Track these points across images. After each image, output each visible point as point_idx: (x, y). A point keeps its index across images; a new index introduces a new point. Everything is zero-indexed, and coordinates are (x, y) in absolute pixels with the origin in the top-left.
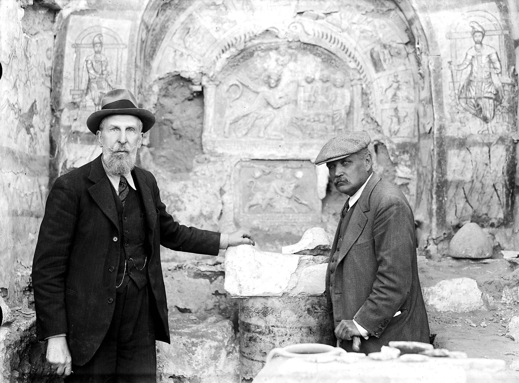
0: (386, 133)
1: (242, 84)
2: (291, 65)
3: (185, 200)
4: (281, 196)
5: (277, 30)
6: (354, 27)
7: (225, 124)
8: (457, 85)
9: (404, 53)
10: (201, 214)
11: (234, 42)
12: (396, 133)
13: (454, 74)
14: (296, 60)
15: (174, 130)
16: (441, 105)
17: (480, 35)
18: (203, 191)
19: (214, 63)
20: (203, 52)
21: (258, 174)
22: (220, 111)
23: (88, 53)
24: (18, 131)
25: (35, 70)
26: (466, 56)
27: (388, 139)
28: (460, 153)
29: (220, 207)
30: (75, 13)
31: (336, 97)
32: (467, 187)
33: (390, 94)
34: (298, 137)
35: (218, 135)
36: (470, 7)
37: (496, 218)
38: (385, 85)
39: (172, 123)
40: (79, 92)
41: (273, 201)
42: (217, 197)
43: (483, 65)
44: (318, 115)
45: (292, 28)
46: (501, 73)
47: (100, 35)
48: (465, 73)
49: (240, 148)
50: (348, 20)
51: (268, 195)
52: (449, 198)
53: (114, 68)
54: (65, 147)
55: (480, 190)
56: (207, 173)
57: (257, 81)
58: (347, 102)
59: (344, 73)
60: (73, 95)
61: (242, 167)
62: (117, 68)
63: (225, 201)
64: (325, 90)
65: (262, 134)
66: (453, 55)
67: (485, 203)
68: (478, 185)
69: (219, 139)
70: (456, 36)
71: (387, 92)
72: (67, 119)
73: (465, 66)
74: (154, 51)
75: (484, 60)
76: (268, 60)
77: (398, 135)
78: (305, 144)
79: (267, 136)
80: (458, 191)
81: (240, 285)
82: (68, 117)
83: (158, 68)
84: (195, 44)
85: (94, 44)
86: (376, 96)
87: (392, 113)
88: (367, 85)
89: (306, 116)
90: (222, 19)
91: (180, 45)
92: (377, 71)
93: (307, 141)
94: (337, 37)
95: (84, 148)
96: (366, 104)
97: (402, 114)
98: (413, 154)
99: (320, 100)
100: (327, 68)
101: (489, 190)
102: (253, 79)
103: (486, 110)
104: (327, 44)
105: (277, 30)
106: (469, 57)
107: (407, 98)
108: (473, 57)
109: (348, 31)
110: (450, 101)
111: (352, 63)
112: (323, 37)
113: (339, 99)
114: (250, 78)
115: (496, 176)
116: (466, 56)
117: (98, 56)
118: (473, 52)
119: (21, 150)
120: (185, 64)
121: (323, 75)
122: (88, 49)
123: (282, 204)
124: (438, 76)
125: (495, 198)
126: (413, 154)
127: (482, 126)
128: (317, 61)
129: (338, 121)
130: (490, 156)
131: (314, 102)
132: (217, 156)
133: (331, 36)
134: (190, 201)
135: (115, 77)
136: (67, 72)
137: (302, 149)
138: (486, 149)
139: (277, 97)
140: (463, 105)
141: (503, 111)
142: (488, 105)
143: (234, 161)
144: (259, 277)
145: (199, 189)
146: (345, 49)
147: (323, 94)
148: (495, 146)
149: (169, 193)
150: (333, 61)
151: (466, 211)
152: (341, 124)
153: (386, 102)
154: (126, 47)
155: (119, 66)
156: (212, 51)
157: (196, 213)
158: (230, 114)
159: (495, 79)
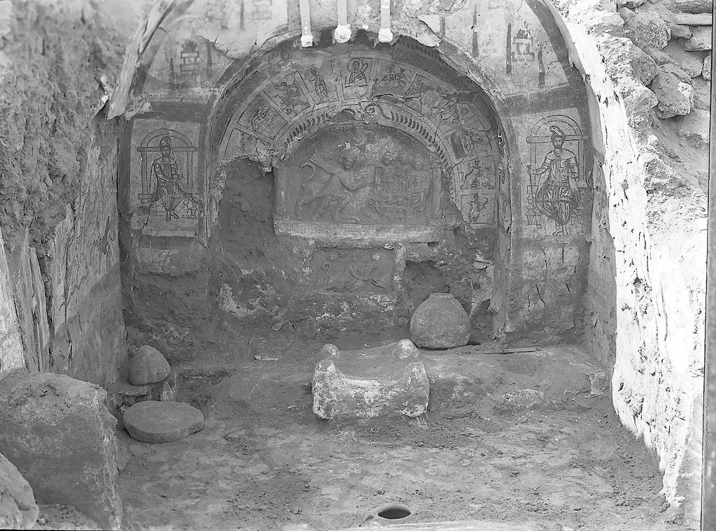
0: (466, 218)
5: (354, 112)
8: (535, 189)
11: (307, 124)
12: (475, 219)
13: (533, 178)
14: (372, 142)
16: (519, 207)
17: (558, 139)
20: (273, 135)
23: (153, 156)
30: (138, 116)
33: (470, 180)
46: (578, 177)
47: (167, 138)
60: (142, 199)
70: (536, 140)
73: (544, 170)
74: (220, 135)
77: (478, 221)
85: (161, 147)
90: (293, 100)
92: (458, 157)
96: (446, 183)
97: (482, 200)
107: (488, 184)
109: (430, 116)
117: (167, 159)
118: (552, 156)
124: (518, 179)
135: (186, 181)
138: (560, 250)
140: (540, 208)
146: (424, 133)
154: (196, 150)
159: (573, 184)
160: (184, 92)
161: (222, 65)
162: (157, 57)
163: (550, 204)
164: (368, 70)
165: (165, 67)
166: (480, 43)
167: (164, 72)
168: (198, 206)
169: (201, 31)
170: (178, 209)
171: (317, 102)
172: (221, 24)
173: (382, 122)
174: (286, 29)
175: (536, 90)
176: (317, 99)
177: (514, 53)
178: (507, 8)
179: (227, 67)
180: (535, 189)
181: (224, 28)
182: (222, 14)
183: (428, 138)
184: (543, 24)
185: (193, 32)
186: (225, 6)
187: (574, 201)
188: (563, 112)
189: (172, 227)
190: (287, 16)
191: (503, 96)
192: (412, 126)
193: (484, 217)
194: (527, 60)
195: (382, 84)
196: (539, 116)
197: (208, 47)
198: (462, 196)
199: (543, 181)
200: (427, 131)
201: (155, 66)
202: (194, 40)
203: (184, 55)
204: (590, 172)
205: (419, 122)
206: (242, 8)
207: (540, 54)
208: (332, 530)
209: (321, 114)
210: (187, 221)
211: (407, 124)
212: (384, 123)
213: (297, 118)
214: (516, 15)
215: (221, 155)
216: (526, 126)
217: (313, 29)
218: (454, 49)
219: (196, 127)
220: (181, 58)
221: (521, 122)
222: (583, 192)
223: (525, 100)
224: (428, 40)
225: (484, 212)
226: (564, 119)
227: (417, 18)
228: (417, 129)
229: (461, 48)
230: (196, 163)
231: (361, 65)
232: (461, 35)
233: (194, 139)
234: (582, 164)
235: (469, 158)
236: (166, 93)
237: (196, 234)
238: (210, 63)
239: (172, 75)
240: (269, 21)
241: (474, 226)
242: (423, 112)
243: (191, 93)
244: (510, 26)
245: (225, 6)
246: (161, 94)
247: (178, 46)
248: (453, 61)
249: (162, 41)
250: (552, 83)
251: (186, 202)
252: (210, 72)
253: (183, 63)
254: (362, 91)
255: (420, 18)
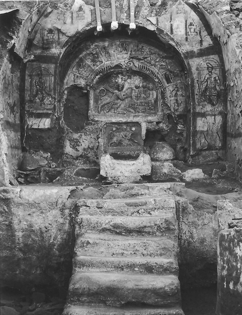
0: (172, 110)
1: (106, 90)
2: (129, 81)
3: (81, 141)
4: (125, 139)
5: (122, 65)
6: (157, 63)
7: (99, 107)
8: (201, 90)
9: (180, 75)
10: (89, 147)
11: (102, 70)
12: (177, 110)
14: (131, 79)
15: (75, 110)
17: (210, 69)
18: (89, 137)
19: (93, 80)
20: (87, 75)
21: (114, 129)
22: (96, 101)
24: (11, 114)
25: (15, 87)
26: (205, 78)
27: (173, 113)
28: (202, 119)
29: (97, 144)
30: (29, 61)
31: (150, 94)
32: (205, 133)
33: (174, 93)
34: (132, 112)
35: (95, 112)
36: (206, 57)
37: (218, 146)
38: (172, 90)
39: (74, 107)
40: (32, 96)
41: (122, 141)
42: (96, 140)
43: (212, 82)
44: (141, 103)
45: (128, 64)
47: (41, 71)
48: (204, 85)
49: (106, 118)
50: (154, 61)
51: (119, 139)
52: (198, 138)
53: (48, 85)
54: (27, 119)
55: (211, 134)
56: (91, 129)
57: (113, 88)
58: (155, 97)
59: (153, 84)
61: (107, 126)
62: (49, 85)
63: (99, 141)
64: (144, 92)
65: (116, 111)
66: (199, 77)
67: (213, 140)
68: (210, 132)
69: (96, 114)
70: (200, 69)
71: (173, 92)
72: (28, 107)
73: (204, 82)
75: (213, 79)
76: (118, 78)
77: (178, 111)
78: (135, 116)
79: (118, 112)
80: (201, 135)
81: (106, 172)
82: (28, 106)
83: (67, 83)
84: (83, 72)
86: (168, 94)
87: (175, 101)
88: (163, 89)
89: (136, 103)
91: (76, 72)
93: (136, 114)
94: (149, 68)
95: (36, 120)
96: (163, 97)
98: (185, 119)
99: (142, 96)
100: (145, 82)
101: (215, 134)
102: (111, 87)
103: (214, 101)
104: (145, 71)
105: (122, 65)
106: (206, 78)
108: (208, 78)
109: (155, 66)
110: (198, 97)
111: (156, 79)
112: (143, 68)
113: (151, 96)
114: (109, 86)
115: (218, 128)
116: (205, 78)
119: (11, 121)
120: (79, 81)
121: (143, 85)
122: (36, 77)
123: (125, 142)
125: (218, 138)
126: (185, 119)
127: (212, 107)
128: (140, 79)
129: (150, 105)
130: (215, 120)
131: (140, 97)
132: (95, 122)
133: (147, 68)
134: (83, 142)
135: (49, 89)
136: (27, 87)
137: (135, 118)
139: (122, 95)
141: (221, 101)
142: (214, 99)
143: (103, 123)
144: (114, 169)
145: (87, 136)
146: (153, 73)
147: (143, 93)
148: (217, 116)
149: (73, 138)
150: (148, 79)
151: (205, 143)
152: (152, 106)
153: (172, 97)
155: (50, 84)
156: (92, 75)
157: (86, 147)
158: (100, 104)
159: (218, 88)
160: (48, 51)
161: (64, 39)
162: (37, 36)
163: (208, 97)
164: (128, 47)
165: (40, 40)
166: (173, 28)
167: (40, 42)
168: (53, 100)
169: (55, 24)
170: (45, 101)
171: (106, 61)
172: (64, 22)
173: (134, 69)
174: (91, 24)
175: (199, 48)
176: (106, 59)
177: (188, 32)
178: (185, 13)
179: (66, 40)
180: (201, 90)
181: (65, 23)
182: (64, 17)
183: (155, 75)
184: (200, 19)
185: (52, 25)
186: (65, 14)
187: (218, 95)
188: (211, 56)
189: (43, 109)
190: (91, 18)
191: (185, 51)
192: (147, 70)
193: (181, 109)
194: (195, 35)
195: (133, 53)
196: (201, 59)
197: (58, 31)
198: (171, 101)
199: (204, 87)
200: (154, 72)
201: (36, 39)
202: (52, 28)
203: (48, 35)
204: (225, 83)
205: (150, 68)
206: (72, 15)
207: (200, 33)
208: (54, 1)
209: (107, 66)
210: (49, 106)
211: (145, 69)
212: (135, 69)
213: (98, 68)
214: (189, 16)
215: (65, 84)
216: (196, 63)
217: (103, 25)
218: (162, 31)
219: (53, 66)
220: (47, 36)
221: (193, 62)
222: (222, 91)
223: (195, 52)
224: (151, 28)
225: (180, 107)
226: (212, 59)
227: (146, 18)
228: (150, 71)
229: (165, 31)
230: (53, 82)
231: (125, 45)
232: (165, 25)
233: (52, 71)
234: (221, 78)
235: (173, 84)
236: (40, 51)
237: (52, 112)
238: (59, 38)
239: (43, 43)
240: (83, 20)
241: (177, 113)
242: (152, 63)
243: (50, 52)
244: (186, 21)
245: (65, 14)
246: (38, 52)
247: (46, 31)
248: (162, 37)
249: (39, 29)
250: (206, 44)
251: (48, 98)
252: (59, 42)
253: (47, 38)
254: (125, 56)
255: (148, 18)
